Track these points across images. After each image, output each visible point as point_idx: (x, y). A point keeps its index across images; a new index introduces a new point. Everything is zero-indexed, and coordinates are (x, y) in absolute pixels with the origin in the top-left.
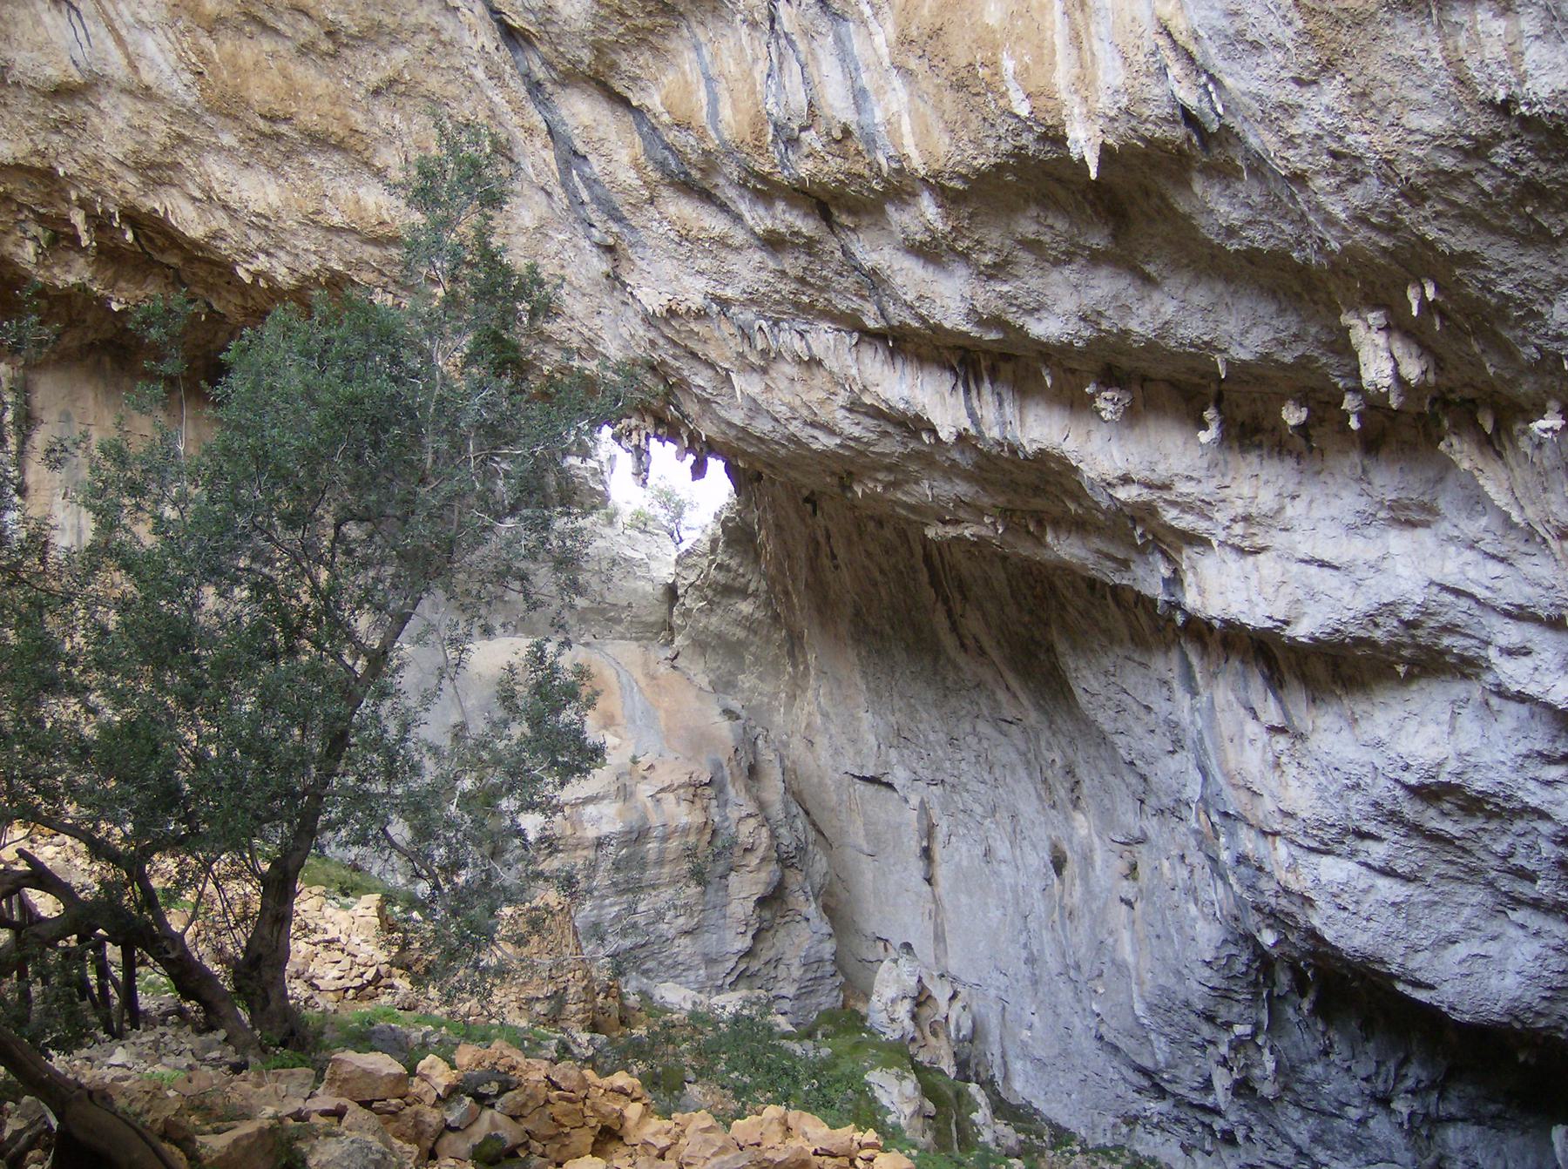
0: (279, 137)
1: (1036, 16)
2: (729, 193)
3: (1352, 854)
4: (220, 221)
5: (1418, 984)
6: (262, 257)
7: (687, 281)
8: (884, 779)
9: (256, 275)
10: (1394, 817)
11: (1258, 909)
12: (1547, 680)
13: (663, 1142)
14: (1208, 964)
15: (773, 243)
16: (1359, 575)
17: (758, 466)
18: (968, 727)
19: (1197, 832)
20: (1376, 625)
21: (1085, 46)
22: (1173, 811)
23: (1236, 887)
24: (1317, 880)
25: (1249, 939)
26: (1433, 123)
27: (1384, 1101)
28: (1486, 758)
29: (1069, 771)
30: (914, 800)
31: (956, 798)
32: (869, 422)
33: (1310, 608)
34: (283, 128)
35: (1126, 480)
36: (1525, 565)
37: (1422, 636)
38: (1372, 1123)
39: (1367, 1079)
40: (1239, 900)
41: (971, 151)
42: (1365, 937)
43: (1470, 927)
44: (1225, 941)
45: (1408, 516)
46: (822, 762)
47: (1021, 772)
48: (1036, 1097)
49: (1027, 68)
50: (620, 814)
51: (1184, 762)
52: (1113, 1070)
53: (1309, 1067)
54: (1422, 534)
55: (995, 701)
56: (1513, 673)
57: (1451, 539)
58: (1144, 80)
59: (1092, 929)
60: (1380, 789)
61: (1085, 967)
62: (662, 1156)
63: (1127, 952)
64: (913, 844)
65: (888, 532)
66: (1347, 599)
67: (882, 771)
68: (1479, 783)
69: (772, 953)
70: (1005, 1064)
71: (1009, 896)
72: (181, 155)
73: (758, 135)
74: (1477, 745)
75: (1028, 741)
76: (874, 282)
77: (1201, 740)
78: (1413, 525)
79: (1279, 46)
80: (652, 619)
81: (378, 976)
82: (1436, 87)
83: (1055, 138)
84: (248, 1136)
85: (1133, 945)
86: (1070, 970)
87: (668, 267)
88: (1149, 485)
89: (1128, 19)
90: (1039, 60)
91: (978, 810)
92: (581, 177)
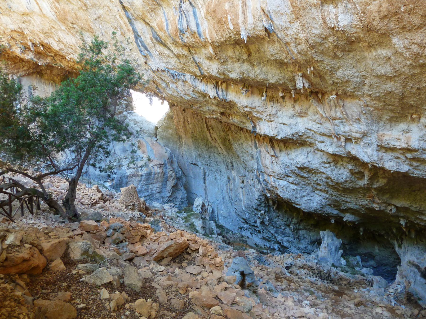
0: (74, 28)
1: (236, 7)
2: (170, 46)
3: (286, 180)
4: (62, 46)
5: (297, 204)
6: (72, 55)
7: (161, 64)
9: (70, 59)
10: (295, 173)
11: (267, 190)
12: (327, 148)
13: (155, 238)
14: (257, 200)
15: (178, 56)
17: (174, 103)
18: (213, 155)
19: (256, 175)
20: (294, 136)
21: (246, 14)
22: (251, 171)
23: (263, 186)
24: (279, 185)
25: (265, 195)
26: (317, 32)
27: (288, 226)
28: (313, 162)
29: (232, 163)
30: (202, 168)
32: (197, 94)
33: (281, 133)
34: (75, 26)
35: (246, 107)
36: (325, 125)
37: (303, 138)
38: (286, 229)
39: (285, 221)
40: (263, 188)
41: (220, 37)
43: (308, 194)
45: (301, 115)
47: (222, 163)
49: (233, 19)
50: (146, 170)
51: (254, 161)
52: (238, 219)
54: (305, 119)
56: (321, 146)
57: (310, 120)
58: (258, 22)
59: (235, 192)
60: (293, 168)
61: (233, 200)
62: (155, 241)
63: (241, 197)
64: (202, 176)
65: (199, 117)
66: (289, 131)
68: (312, 167)
69: (175, 196)
70: (218, 217)
71: (219, 186)
72: (53, 31)
73: (176, 32)
75: (224, 157)
76: (198, 65)
77: (258, 158)
78: (302, 116)
79: (286, 14)
80: (153, 133)
81: (96, 201)
82: (319, 24)
83: (238, 34)
84: (56, 243)
86: (231, 200)
87: (157, 61)
88: (251, 108)
89: (255, 8)
90: (236, 17)
91: (214, 170)
92: (140, 41)
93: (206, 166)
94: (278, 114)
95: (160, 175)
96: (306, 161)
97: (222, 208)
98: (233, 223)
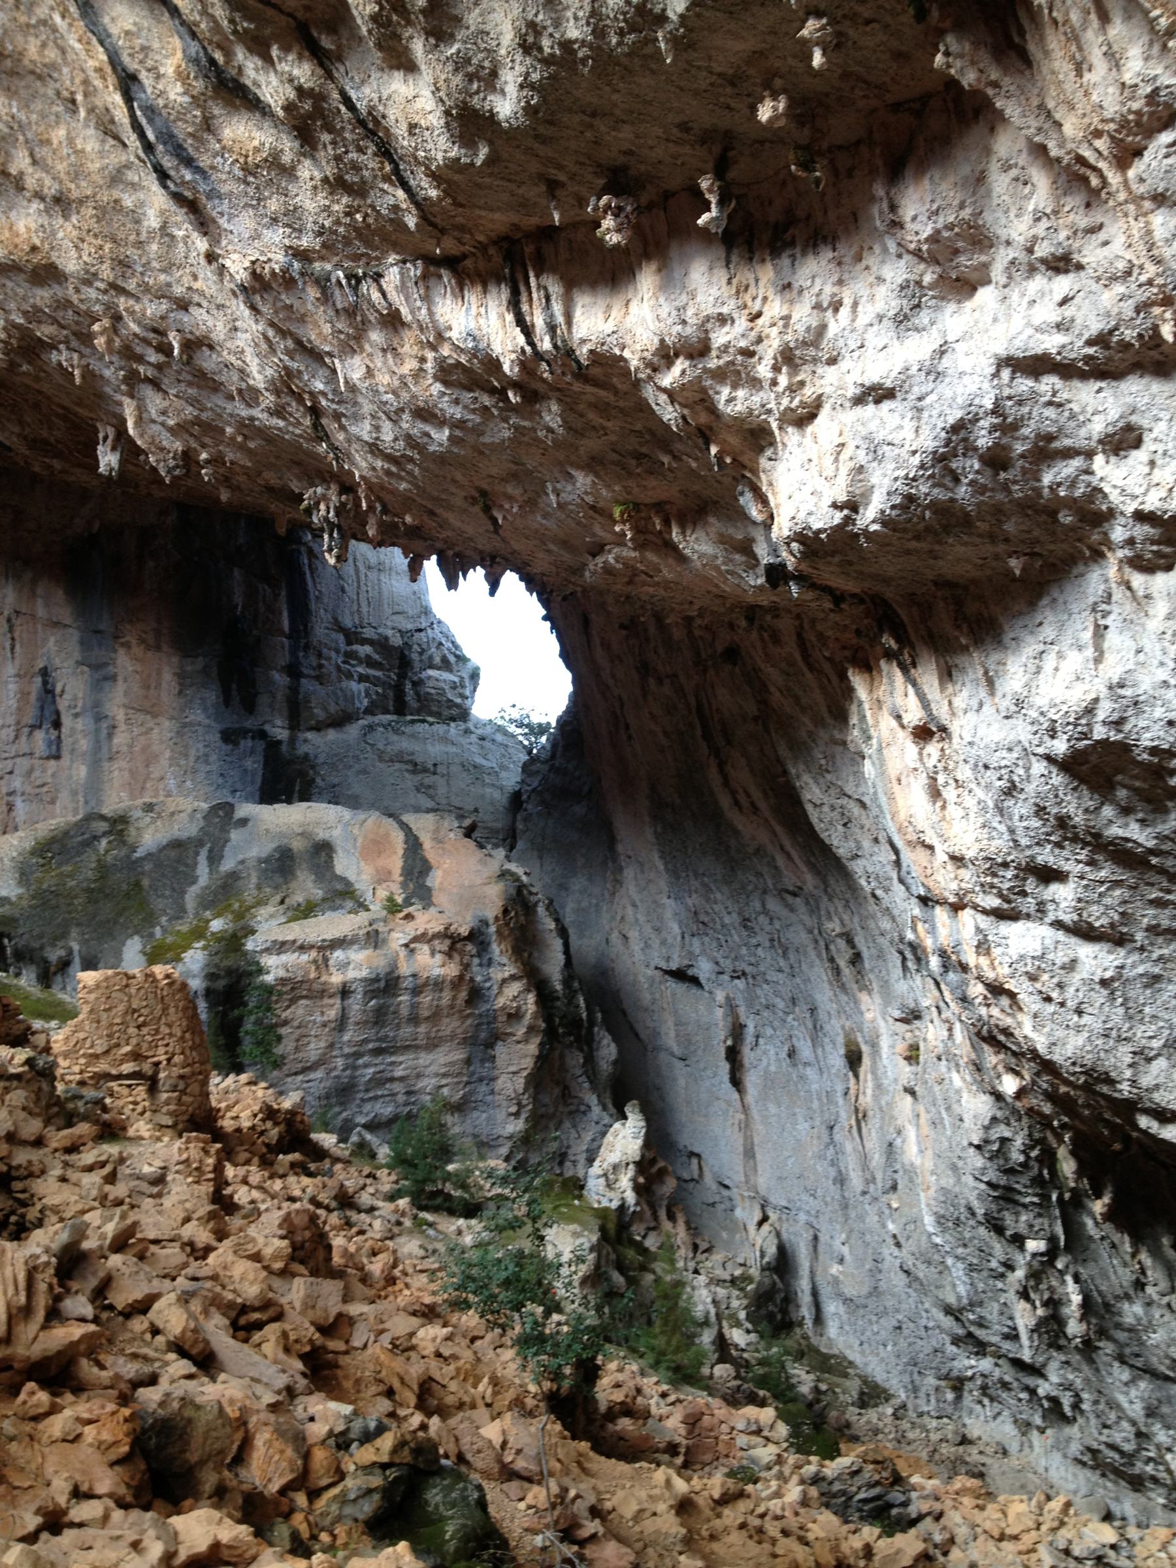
8: (690, 972)
16: (917, 391)
18: (757, 905)
30: (720, 996)
31: (759, 992)
42: (1080, 1040)
44: (994, 1120)
46: (636, 959)
48: (851, 1347)
53: (1126, 1306)
55: (776, 868)
67: (686, 962)
74: (1130, 666)
80: (499, 825)
85: (919, 1143)
91: (781, 1004)
93: (740, 984)
94: (833, 329)
95: (447, 996)
96: (1098, 687)
97: (837, 1243)
98: (903, 1344)
